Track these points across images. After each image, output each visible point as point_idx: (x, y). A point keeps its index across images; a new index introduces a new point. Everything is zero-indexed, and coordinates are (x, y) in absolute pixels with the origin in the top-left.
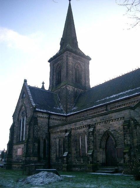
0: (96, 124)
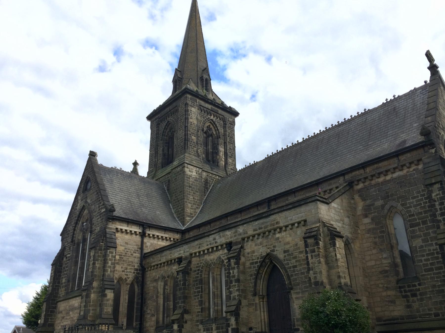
0: (243, 239)
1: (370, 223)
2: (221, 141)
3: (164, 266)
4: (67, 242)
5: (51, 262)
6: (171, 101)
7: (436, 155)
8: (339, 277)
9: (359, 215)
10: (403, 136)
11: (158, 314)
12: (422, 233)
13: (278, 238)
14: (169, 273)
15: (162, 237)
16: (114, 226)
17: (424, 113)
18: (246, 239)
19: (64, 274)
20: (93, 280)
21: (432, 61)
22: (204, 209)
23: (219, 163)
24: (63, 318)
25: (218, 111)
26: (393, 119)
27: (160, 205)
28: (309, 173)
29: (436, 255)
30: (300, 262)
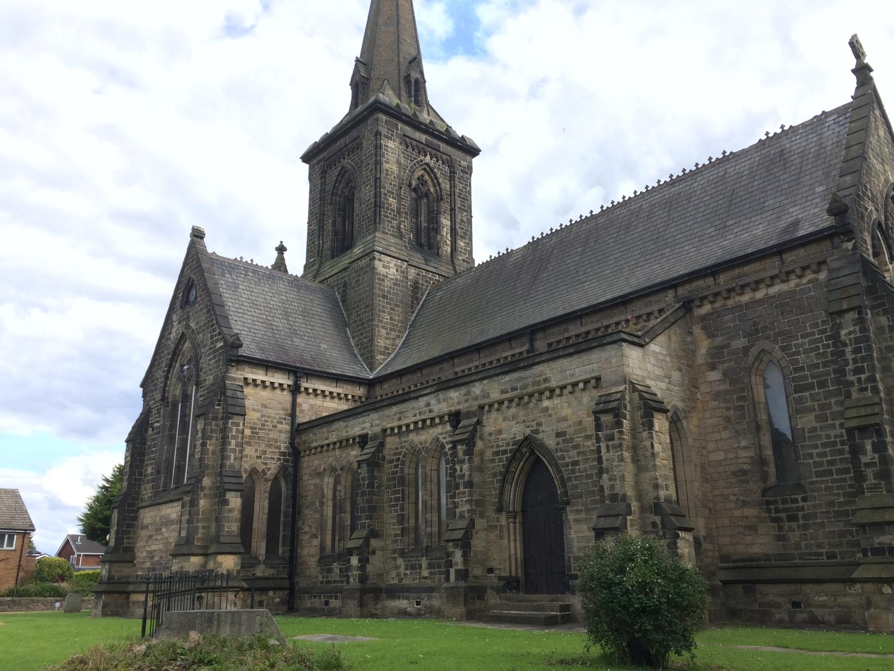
0: (482, 407)
1: (720, 380)
2: (445, 206)
3: (334, 449)
4: (154, 399)
5: (126, 436)
7: (854, 254)
8: (656, 487)
9: (700, 365)
10: (795, 212)
11: (323, 535)
12: (816, 404)
14: (344, 462)
15: (331, 393)
16: (241, 375)
17: (839, 166)
18: (487, 408)
19: (150, 459)
20: (202, 475)
21: (861, 55)
22: (412, 340)
23: (440, 250)
24: (150, 537)
25: (439, 146)
26: (777, 175)
27: (328, 331)
28: (609, 279)
29: (839, 447)
30: (585, 455)
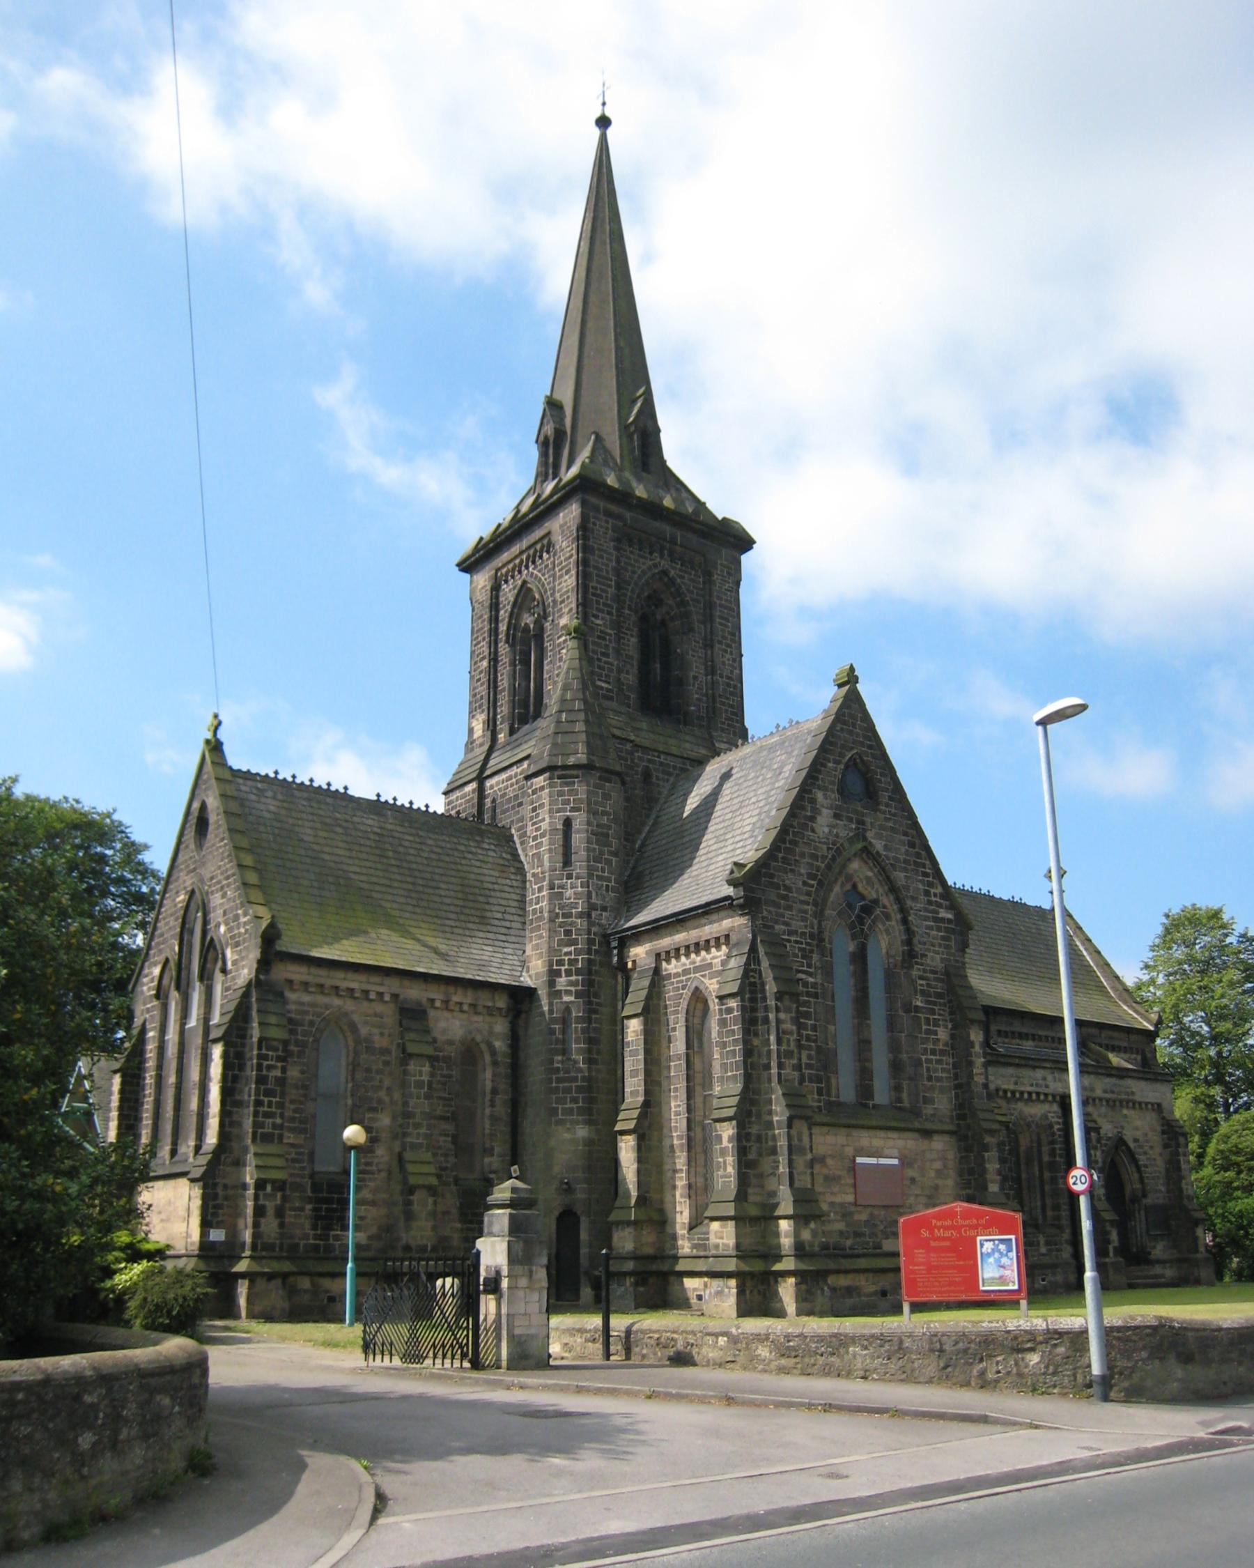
6: (504, 682)
13: (1126, 1116)
